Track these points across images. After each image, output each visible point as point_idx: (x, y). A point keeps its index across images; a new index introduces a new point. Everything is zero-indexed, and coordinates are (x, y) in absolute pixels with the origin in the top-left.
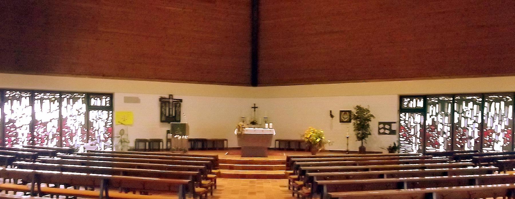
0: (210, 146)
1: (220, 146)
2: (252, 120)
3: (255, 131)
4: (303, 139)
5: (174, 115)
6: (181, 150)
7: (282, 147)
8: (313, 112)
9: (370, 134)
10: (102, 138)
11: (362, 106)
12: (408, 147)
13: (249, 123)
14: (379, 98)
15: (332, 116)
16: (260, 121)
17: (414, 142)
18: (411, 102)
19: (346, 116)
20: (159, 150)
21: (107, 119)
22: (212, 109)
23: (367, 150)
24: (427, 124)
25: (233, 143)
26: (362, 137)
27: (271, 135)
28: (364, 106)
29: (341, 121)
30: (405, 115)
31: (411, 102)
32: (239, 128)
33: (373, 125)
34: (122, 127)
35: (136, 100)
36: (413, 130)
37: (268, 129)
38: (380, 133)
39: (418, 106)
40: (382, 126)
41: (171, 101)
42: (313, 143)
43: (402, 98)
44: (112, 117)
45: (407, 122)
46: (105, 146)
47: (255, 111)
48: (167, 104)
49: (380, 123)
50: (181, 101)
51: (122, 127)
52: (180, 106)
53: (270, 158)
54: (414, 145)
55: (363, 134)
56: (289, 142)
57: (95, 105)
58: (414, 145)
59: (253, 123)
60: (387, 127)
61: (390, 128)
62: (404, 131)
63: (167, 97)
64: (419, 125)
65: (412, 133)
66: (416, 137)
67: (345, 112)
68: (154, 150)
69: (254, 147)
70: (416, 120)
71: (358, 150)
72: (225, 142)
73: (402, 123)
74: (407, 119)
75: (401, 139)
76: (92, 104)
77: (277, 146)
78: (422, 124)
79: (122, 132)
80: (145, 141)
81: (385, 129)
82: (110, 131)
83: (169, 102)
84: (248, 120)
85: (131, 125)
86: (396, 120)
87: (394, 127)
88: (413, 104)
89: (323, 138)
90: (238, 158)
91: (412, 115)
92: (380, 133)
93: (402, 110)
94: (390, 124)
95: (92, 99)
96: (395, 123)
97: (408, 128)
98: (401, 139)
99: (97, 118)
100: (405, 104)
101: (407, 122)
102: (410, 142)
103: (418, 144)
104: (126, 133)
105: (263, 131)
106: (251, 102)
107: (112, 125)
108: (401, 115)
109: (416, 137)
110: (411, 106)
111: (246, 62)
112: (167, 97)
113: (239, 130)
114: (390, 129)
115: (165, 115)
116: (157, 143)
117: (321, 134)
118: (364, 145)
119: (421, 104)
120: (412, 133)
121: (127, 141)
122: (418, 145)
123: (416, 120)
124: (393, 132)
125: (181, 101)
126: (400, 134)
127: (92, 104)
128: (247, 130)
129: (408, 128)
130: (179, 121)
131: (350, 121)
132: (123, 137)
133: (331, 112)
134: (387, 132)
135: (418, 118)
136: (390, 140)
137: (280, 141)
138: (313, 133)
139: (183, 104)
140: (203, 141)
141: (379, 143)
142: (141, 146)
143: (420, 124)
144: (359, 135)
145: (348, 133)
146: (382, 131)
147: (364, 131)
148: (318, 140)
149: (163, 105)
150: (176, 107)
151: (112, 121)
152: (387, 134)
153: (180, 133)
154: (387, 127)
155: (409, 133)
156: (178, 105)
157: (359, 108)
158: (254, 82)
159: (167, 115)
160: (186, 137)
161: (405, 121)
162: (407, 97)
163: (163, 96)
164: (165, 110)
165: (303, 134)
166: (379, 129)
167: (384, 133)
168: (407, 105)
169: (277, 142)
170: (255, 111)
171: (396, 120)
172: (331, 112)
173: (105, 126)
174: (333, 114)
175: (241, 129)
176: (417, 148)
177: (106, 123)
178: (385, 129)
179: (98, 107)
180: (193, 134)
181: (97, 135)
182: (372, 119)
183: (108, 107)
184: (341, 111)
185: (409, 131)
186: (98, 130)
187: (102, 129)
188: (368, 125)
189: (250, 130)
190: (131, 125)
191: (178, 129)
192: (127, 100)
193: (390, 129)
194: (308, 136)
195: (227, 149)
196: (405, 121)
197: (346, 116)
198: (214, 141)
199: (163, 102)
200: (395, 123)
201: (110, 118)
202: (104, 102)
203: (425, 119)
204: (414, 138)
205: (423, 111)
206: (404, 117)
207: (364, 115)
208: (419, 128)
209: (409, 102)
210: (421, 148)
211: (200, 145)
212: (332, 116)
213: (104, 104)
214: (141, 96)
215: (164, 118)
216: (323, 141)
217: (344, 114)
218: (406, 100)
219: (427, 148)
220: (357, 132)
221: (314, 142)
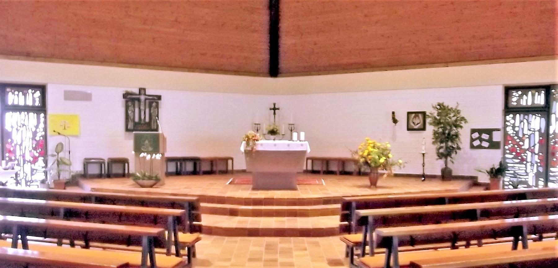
0: (205, 167)
1: (221, 167)
2: (271, 128)
3: (275, 145)
4: (356, 157)
5: (147, 120)
6: (150, 178)
7: (316, 168)
8: (367, 115)
9: (459, 148)
10: (28, 157)
11: (446, 104)
12: (520, 169)
13: (265, 132)
14: (474, 93)
15: (395, 121)
16: (283, 129)
17: (529, 159)
18: (525, 96)
19: (417, 121)
20: (123, 175)
21: (37, 127)
22: (202, 111)
23: (454, 174)
24: (551, 132)
25: (240, 163)
26: (446, 154)
27: (304, 152)
28: (450, 104)
29: (409, 129)
30: (514, 118)
31: (525, 96)
32: (248, 139)
33: (464, 135)
34: (60, 139)
35: (87, 97)
36: (527, 141)
37: (298, 143)
38: (472, 147)
39: (536, 102)
40: (476, 135)
41: (143, 98)
42: (373, 165)
43: (508, 90)
44: (45, 123)
45: (517, 129)
46: (32, 170)
47: (275, 113)
48: (136, 103)
49: (473, 131)
50: (159, 98)
51: (60, 139)
52: (157, 107)
53: (302, 193)
54: (529, 164)
55: (447, 148)
56: (327, 161)
57: (16, 103)
58: (529, 164)
59: (273, 132)
60: (485, 136)
61: (491, 137)
62: (513, 144)
63: (136, 91)
64: (537, 134)
65: (526, 146)
66: (533, 152)
67: (417, 113)
68: (117, 176)
69: (273, 171)
70: (532, 126)
71: (439, 173)
72: (230, 162)
73: (510, 130)
74: (517, 124)
75: (507, 156)
76: (10, 103)
77: (310, 168)
78: (543, 131)
79: (60, 148)
80: (100, 163)
81: (481, 140)
82: (42, 147)
83: (139, 100)
84: (265, 128)
85: (76, 137)
86: (500, 126)
87: (497, 137)
88: (527, 100)
89: (390, 155)
90: (246, 193)
91: (526, 117)
92: (472, 147)
93: (508, 110)
94: (489, 132)
95: (10, 93)
96: (498, 130)
97: (519, 138)
98: (507, 156)
99: (19, 125)
100: (514, 99)
101: (517, 129)
102: (522, 161)
103: (537, 163)
104: (66, 148)
105: (289, 145)
106: (270, 100)
107: (45, 137)
108: (508, 118)
109: (533, 152)
110: (523, 103)
111: (264, 55)
112: (136, 91)
113: (248, 144)
114: (490, 140)
115: (134, 120)
116: (121, 166)
117: (385, 149)
118: (450, 165)
119: (540, 99)
120: (526, 146)
121: (67, 162)
122: (535, 165)
123: (532, 126)
124: (494, 145)
125: (159, 98)
126: (506, 147)
127: (10, 103)
128: (262, 145)
129: (519, 138)
130: (157, 130)
131: (423, 129)
132: (61, 155)
133: (393, 113)
134: (485, 144)
135: (537, 122)
136: (493, 158)
137: (313, 160)
138: (374, 147)
139: (162, 103)
140: (195, 161)
141: (475, 162)
142: (94, 170)
143: (540, 131)
144: (441, 151)
145: (423, 148)
146: (476, 143)
147: (450, 144)
148: (382, 160)
149: (130, 104)
150: (150, 107)
151: (45, 130)
152: (485, 148)
153: (150, 149)
154: (484, 137)
155: (520, 146)
156: (154, 104)
157: (442, 109)
158: (274, 71)
159: (137, 120)
160: (158, 156)
161: (514, 127)
162: (517, 88)
163: (130, 90)
164: (134, 112)
165: (355, 150)
166: (472, 140)
167: (480, 147)
168: (518, 101)
169: (310, 162)
170: (275, 113)
171: (500, 126)
172: (393, 113)
173: (34, 139)
174: (396, 118)
175: (251, 143)
176: (535, 171)
177: (35, 134)
178: (481, 140)
179: (21, 106)
180: (174, 150)
181: (18, 153)
182: (463, 124)
183: (38, 107)
184: (409, 113)
185: (521, 143)
186: (21, 145)
187: (29, 144)
188: (457, 135)
189: (266, 144)
190: (76, 137)
191: (147, 142)
192: (69, 96)
193: (490, 140)
194: (366, 154)
195: (232, 172)
196: (514, 127)
197: (416, 121)
198: (212, 161)
199: (130, 99)
200: (498, 130)
201: (42, 125)
202: (32, 98)
203: (548, 124)
204: (529, 154)
205: (545, 111)
206: (512, 121)
207: (450, 118)
208: (537, 138)
209: (521, 97)
210: (541, 169)
211: (189, 167)
212: (395, 121)
213: (30, 103)
214: (95, 91)
215: (130, 126)
216: (390, 160)
217: (415, 117)
218: (516, 95)
219: (552, 169)
220: (438, 145)
221: (376, 162)
